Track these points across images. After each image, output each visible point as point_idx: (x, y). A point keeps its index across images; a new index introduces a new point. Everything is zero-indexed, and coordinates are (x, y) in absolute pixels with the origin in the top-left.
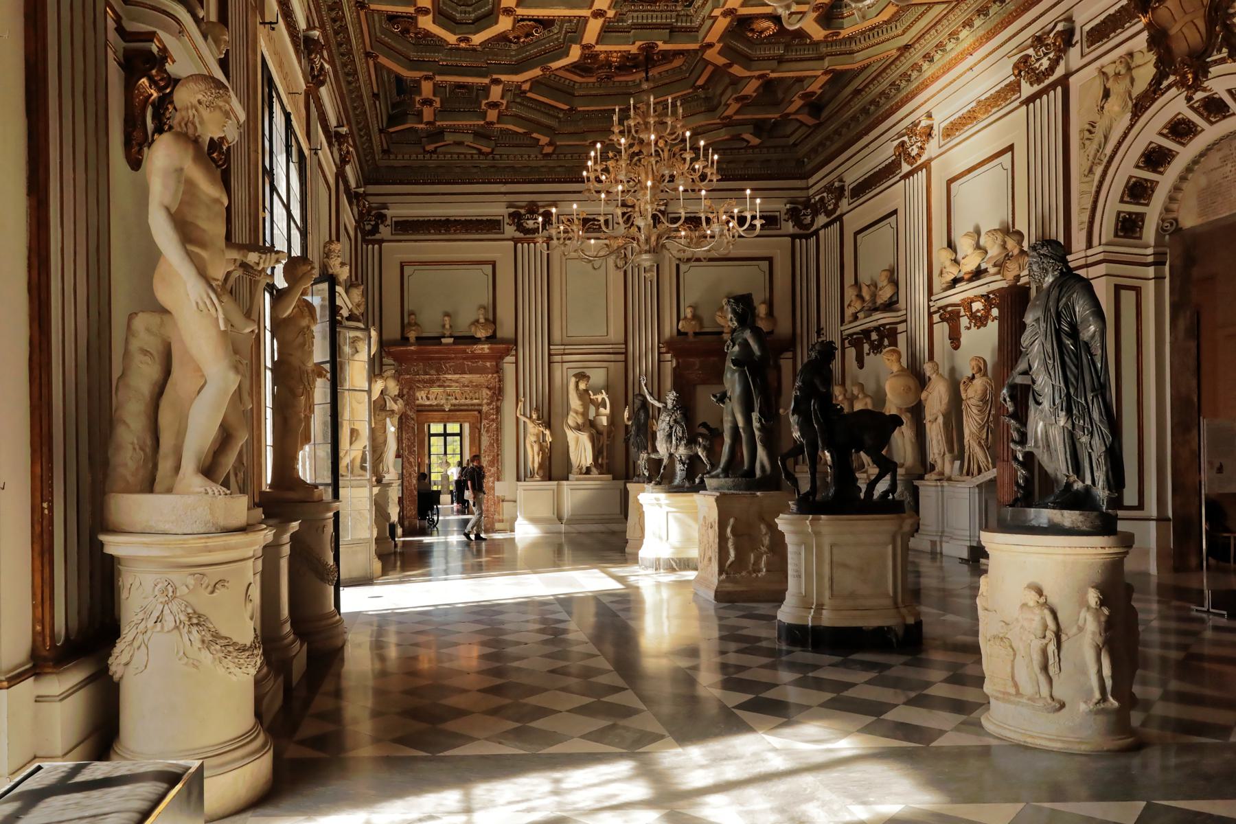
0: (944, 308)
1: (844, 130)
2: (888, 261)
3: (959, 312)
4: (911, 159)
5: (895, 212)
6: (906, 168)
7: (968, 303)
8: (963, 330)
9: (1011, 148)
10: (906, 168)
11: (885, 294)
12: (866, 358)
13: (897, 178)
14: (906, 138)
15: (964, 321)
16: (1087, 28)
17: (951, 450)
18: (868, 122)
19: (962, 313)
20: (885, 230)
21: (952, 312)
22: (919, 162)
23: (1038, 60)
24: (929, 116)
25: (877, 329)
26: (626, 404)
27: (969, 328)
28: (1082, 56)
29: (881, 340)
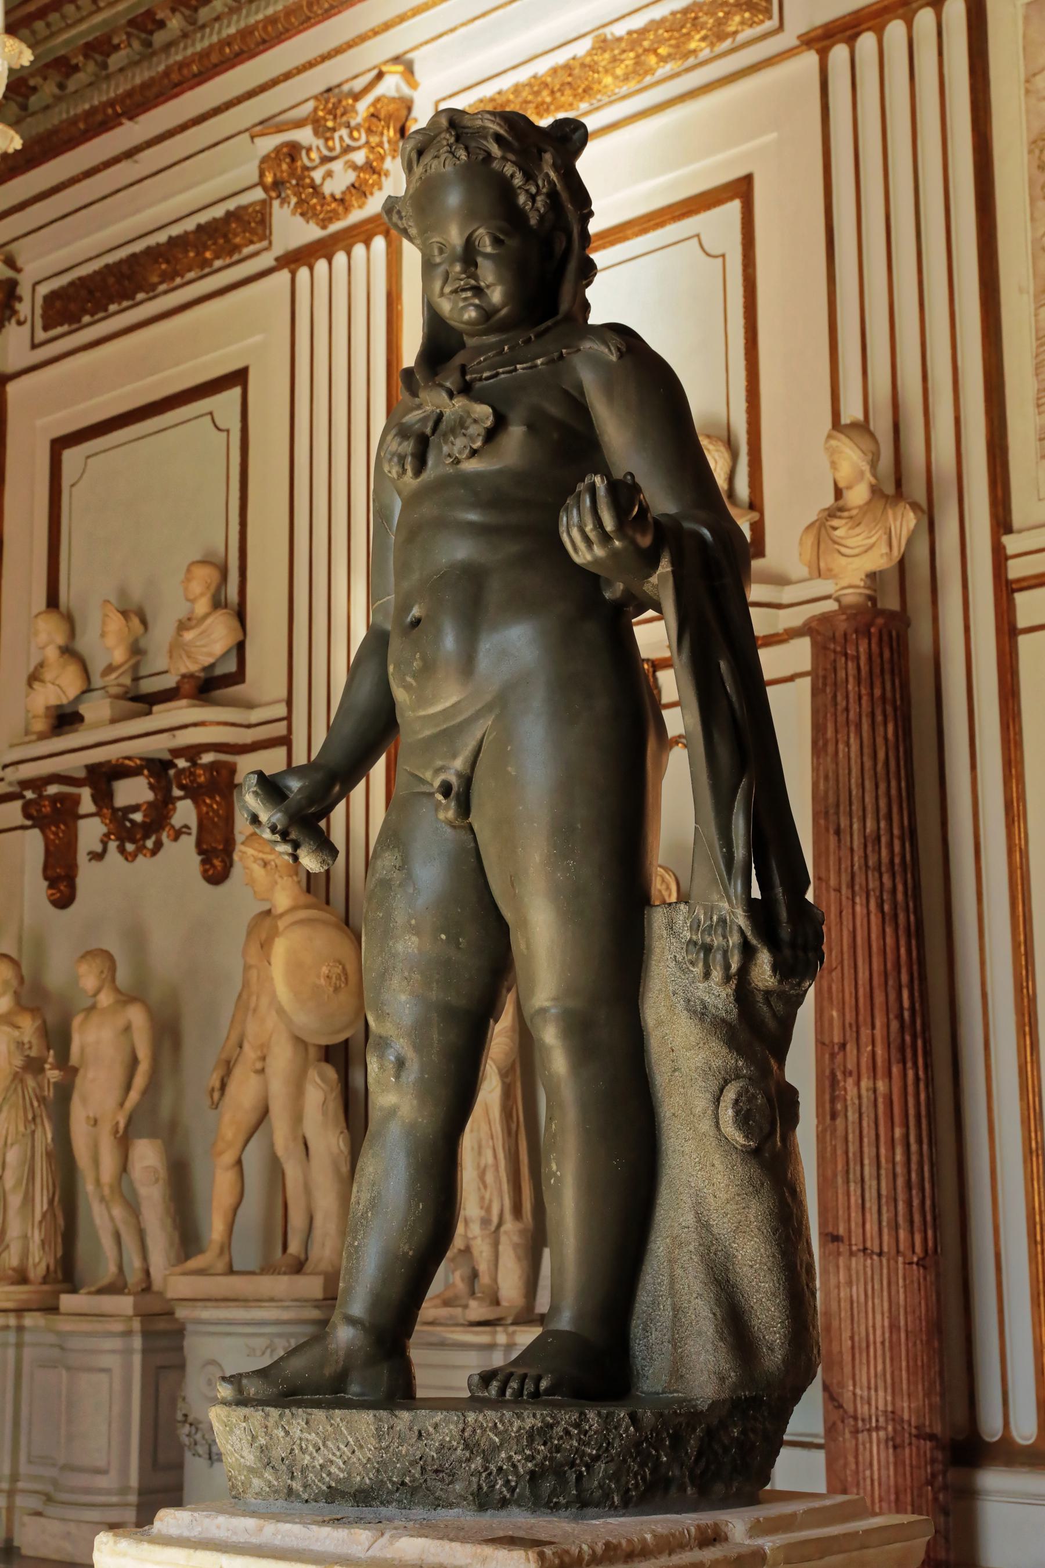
0: (38, 784)
1: (49, 89)
2: (217, 534)
3: (76, 800)
4: (313, 203)
5: (239, 378)
6: (291, 229)
7: (103, 778)
8: (82, 858)
9: (742, 189)
10: (291, 229)
11: (213, 641)
12: (87, 874)
13: (266, 260)
14: (305, 136)
15: (91, 831)
16: (43, 290)
17: (517, 1210)
18: (140, 76)
19: (87, 805)
20: (194, 440)
21: (213, 766)
22: (356, 216)
23: (325, 160)
24: (405, 64)
25: (157, 769)
26: (882, 653)
27: (97, 857)
28: (34, 346)
29: (159, 815)
